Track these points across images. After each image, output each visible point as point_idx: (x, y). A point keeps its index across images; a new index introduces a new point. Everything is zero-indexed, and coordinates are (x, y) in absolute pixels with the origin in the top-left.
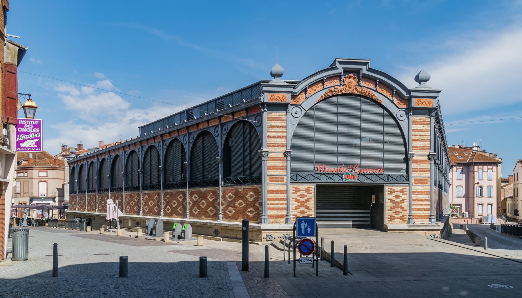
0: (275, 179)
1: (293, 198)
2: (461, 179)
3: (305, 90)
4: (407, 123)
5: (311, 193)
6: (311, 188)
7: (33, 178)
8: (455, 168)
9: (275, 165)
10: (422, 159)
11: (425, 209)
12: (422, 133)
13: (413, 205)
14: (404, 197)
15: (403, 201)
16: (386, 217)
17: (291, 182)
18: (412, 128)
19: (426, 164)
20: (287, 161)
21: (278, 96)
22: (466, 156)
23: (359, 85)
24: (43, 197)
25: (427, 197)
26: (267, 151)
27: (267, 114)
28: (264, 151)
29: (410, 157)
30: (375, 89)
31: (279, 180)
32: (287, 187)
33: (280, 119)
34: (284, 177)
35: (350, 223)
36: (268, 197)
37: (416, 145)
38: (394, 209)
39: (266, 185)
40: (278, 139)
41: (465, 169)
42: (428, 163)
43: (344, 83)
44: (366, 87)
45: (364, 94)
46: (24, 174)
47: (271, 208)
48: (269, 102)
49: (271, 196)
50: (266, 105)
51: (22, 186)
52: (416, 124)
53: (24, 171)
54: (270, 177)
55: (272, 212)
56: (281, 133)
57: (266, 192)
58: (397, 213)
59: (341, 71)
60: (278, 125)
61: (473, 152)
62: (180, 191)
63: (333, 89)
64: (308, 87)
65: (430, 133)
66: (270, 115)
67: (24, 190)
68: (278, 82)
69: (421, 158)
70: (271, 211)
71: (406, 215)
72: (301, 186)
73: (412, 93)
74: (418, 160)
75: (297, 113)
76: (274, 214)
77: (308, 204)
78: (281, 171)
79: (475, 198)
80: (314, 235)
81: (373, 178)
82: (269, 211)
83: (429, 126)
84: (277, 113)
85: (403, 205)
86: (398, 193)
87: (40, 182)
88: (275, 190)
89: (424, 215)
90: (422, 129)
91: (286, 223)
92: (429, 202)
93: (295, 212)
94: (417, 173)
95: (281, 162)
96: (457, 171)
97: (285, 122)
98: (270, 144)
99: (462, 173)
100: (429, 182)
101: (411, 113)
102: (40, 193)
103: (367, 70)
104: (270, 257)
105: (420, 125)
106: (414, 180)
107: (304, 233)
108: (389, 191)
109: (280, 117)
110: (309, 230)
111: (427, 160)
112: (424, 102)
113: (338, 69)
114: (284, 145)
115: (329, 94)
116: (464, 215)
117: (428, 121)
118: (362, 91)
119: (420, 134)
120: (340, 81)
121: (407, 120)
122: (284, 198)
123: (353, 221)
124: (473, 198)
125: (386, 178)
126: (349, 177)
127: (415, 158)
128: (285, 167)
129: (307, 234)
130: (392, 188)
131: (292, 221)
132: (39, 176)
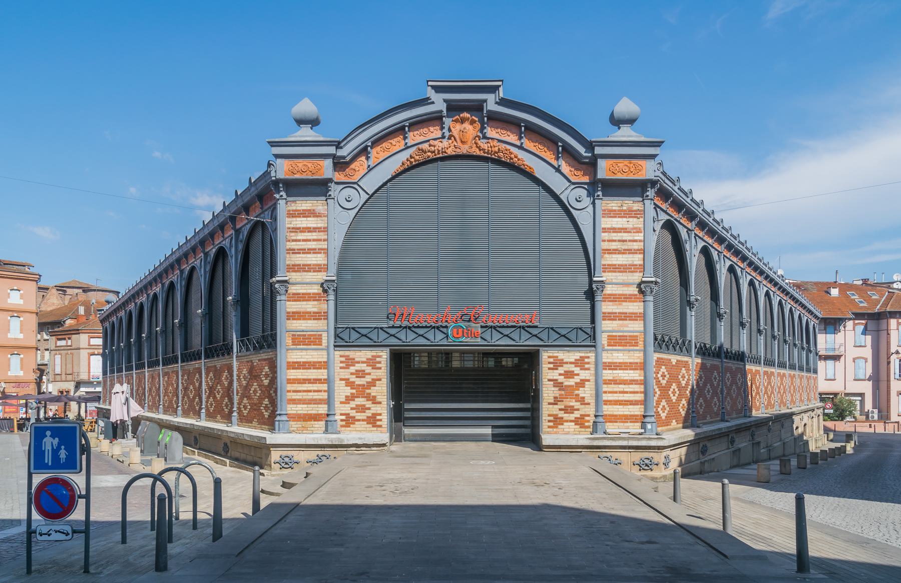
0: (303, 339)
1: (341, 380)
2: (863, 344)
3: (364, 151)
4: (592, 215)
5: (380, 368)
6: (380, 357)
7: (79, 349)
8: (850, 324)
9: (302, 310)
10: (625, 292)
11: (632, 401)
12: (626, 236)
13: (605, 392)
14: (584, 375)
15: (582, 384)
16: (544, 418)
17: (336, 344)
18: (603, 226)
19: (635, 304)
20: (327, 301)
21: (305, 165)
22: (875, 299)
23: (485, 137)
24: (95, 382)
25: (637, 375)
26: (286, 281)
27: (286, 203)
28: (278, 282)
29: (598, 289)
30: (518, 143)
31: (312, 342)
32: (328, 354)
33: (312, 213)
34: (321, 335)
35: (488, 431)
36: (289, 377)
37: (610, 263)
38: (563, 401)
39: (284, 351)
40: (309, 256)
41: (872, 325)
42: (640, 302)
43: (451, 133)
44: (499, 141)
45: (495, 156)
46: (67, 342)
47: (294, 400)
48: (287, 177)
49: (294, 374)
50: (281, 185)
51: (64, 362)
52: (611, 217)
53: (66, 337)
54: (293, 335)
55: (297, 409)
56: (315, 243)
57: (284, 366)
58: (568, 410)
59: (443, 107)
60: (309, 225)
61: (889, 292)
62: (197, 367)
63: (425, 146)
65: (642, 234)
66: (293, 205)
67: (66, 369)
68: (307, 136)
69: (623, 290)
70: (295, 406)
71: (588, 416)
72: (358, 354)
73: (596, 148)
74: (615, 295)
75: (350, 199)
76: (301, 412)
77: (373, 391)
78: (316, 321)
79: (891, 382)
80: (76, 469)
81: (515, 335)
82: (291, 406)
83: (642, 220)
84: (308, 202)
85: (581, 392)
86: (572, 368)
87: (91, 355)
88: (303, 362)
89: (631, 416)
90: (625, 226)
91: (326, 431)
92: (643, 386)
93: (345, 409)
94: (614, 322)
95: (316, 303)
96: (854, 330)
97: (324, 218)
98: (303, 265)
99: (865, 332)
100: (640, 343)
101: (600, 193)
102: (91, 374)
103: (496, 103)
104: (225, 504)
105: (620, 219)
106: (608, 339)
107: (50, 464)
108: (550, 363)
109: (314, 210)
110: (63, 454)
111: (636, 295)
112: (626, 167)
113: (433, 103)
114: (322, 268)
115: (417, 158)
116: (870, 415)
117: (640, 208)
118: (490, 149)
119: (621, 239)
120: (442, 128)
121: (592, 208)
122: (321, 380)
123: (493, 427)
124: (888, 381)
125: (544, 336)
126: (460, 333)
127: (609, 290)
128: (324, 313)
129: (57, 464)
130: (557, 357)
131: (339, 426)
132: (89, 345)
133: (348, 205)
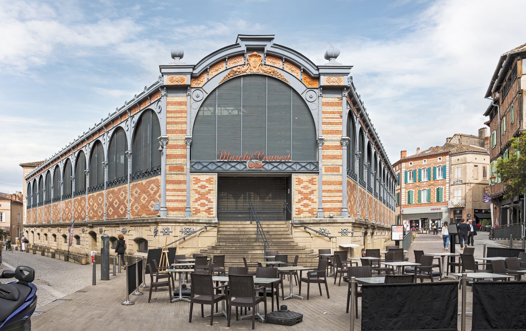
26: (322, 139)
30: (281, 68)
63: (235, 69)
64: (209, 67)
72: (202, 176)
113: (240, 46)
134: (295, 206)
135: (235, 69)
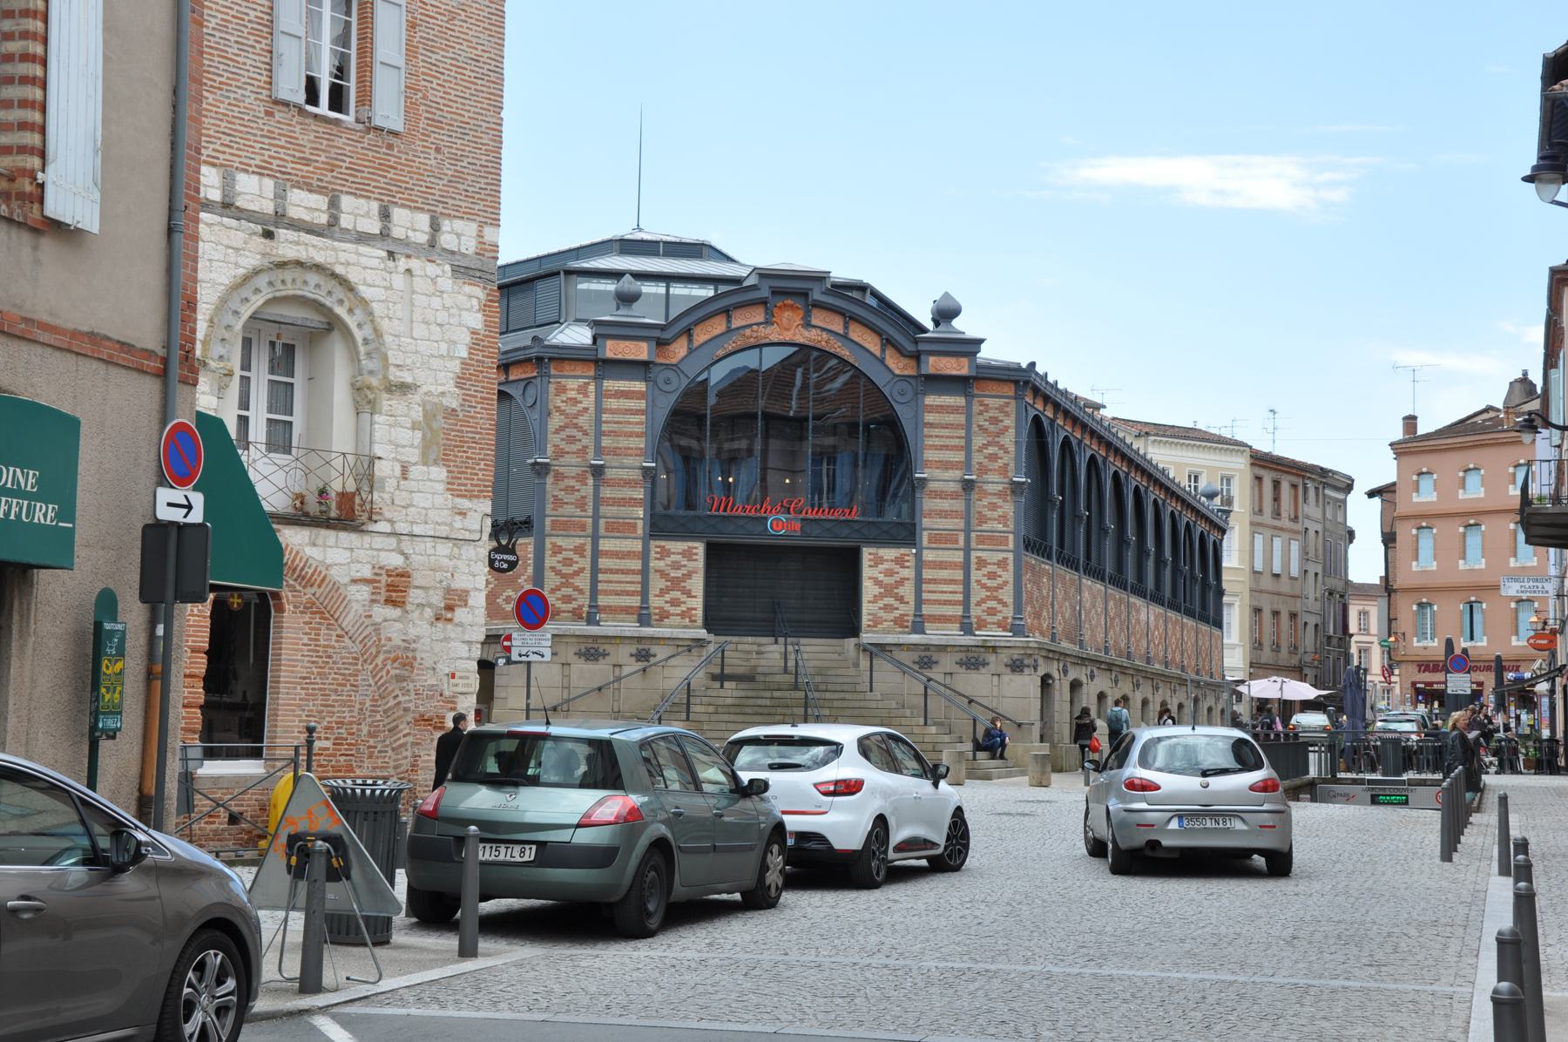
86: (571, 554)
133: (667, 388)
134: (867, 608)
135: (748, 332)
